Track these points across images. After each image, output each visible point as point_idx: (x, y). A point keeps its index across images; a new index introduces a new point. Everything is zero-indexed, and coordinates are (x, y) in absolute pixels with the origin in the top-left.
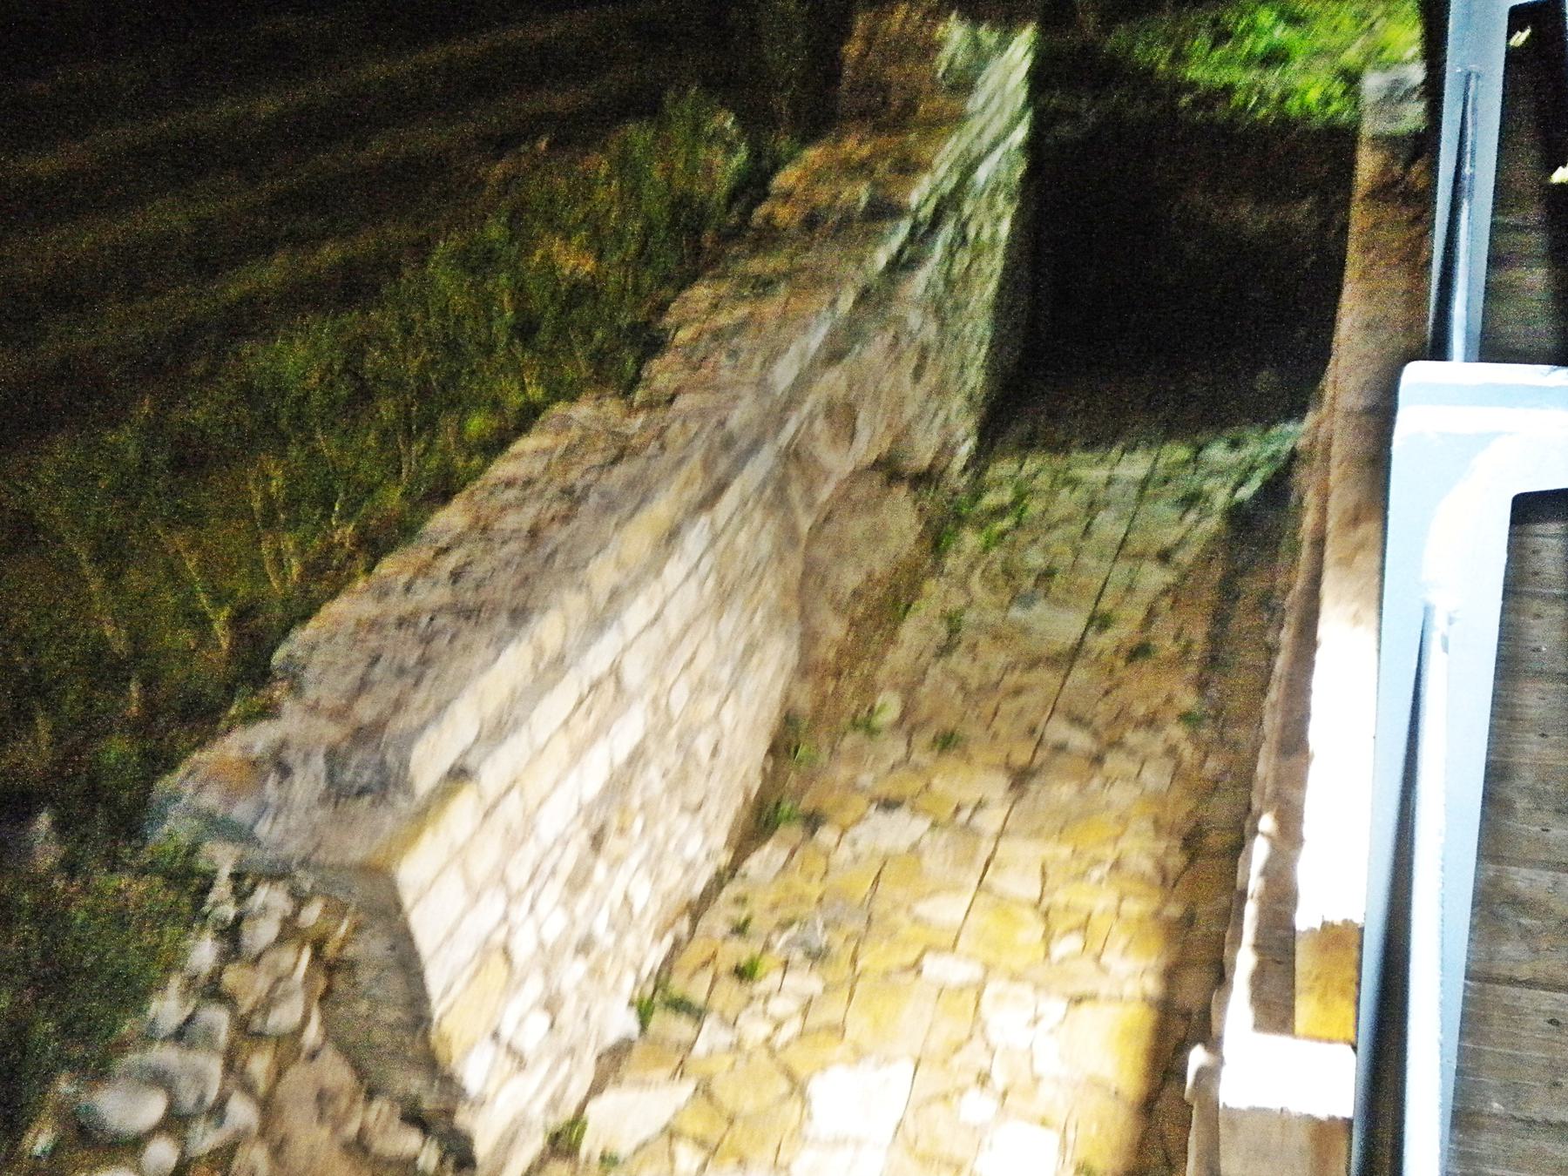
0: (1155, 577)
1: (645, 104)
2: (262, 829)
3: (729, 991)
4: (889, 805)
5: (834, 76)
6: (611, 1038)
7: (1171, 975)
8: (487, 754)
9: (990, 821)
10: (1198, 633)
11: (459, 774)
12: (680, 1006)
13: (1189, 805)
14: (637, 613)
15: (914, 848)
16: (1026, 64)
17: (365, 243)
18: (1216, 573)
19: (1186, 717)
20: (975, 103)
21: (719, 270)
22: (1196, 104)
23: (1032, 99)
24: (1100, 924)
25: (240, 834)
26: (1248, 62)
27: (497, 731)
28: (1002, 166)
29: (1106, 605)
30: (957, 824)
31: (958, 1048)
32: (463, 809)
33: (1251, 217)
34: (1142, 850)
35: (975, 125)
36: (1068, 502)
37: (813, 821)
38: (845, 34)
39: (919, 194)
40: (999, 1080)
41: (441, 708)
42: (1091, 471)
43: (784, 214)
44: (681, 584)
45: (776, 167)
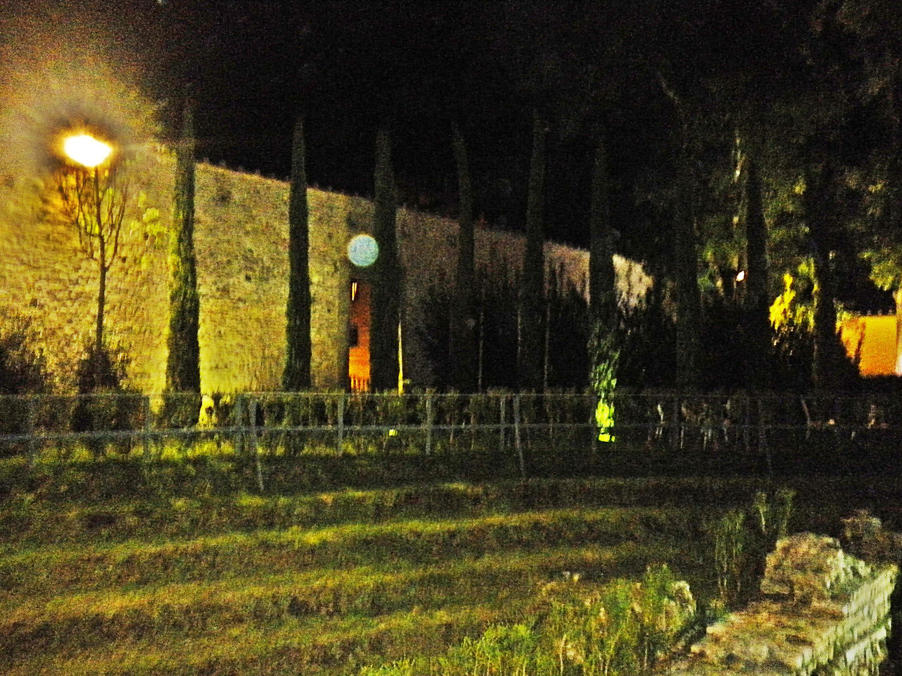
1: (632, 568)
5: (759, 570)
16: (891, 589)
17: (462, 615)
21: (78, 587)
23: (892, 612)
35: (848, 623)
38: (771, 549)
43: (714, 653)
45: (713, 620)
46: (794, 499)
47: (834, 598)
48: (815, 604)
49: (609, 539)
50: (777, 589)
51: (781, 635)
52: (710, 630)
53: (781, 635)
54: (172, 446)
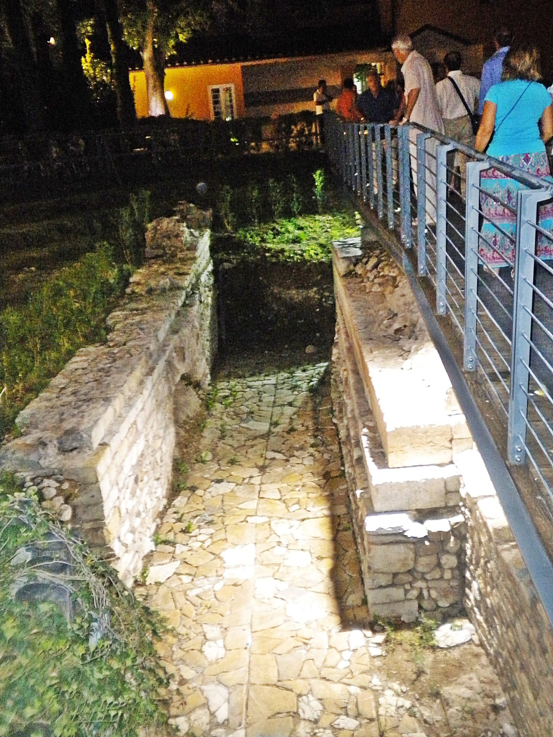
0: (289, 411)
2: (42, 462)
3: (181, 537)
4: (219, 481)
6: (146, 552)
7: (331, 509)
8: (111, 438)
9: (256, 480)
10: (310, 423)
11: (104, 445)
12: (166, 542)
13: (322, 468)
14: (139, 405)
15: (232, 491)
18: (310, 405)
19: (312, 446)
20: (197, 254)
22: (272, 256)
23: (212, 256)
24: (303, 501)
25: (36, 465)
26: (288, 242)
27: (111, 433)
28: (206, 279)
29: (274, 419)
30: (246, 482)
31: (268, 538)
32: (108, 453)
33: (295, 295)
34: (311, 481)
36: (249, 393)
37: (193, 489)
39: (187, 282)
40: (284, 543)
41: (96, 422)
42: (256, 382)
44: (145, 401)
45: (130, 275)
46: (151, 196)
47: (188, 249)
48: (180, 255)
49: (41, 241)
50: (156, 252)
51: (171, 273)
52: (131, 280)
53: (171, 273)
54: (404, 41)
